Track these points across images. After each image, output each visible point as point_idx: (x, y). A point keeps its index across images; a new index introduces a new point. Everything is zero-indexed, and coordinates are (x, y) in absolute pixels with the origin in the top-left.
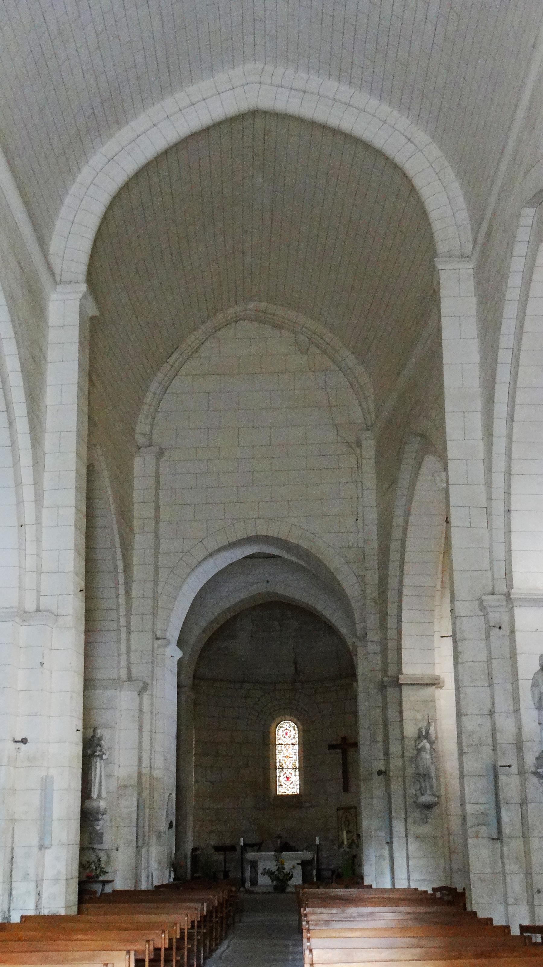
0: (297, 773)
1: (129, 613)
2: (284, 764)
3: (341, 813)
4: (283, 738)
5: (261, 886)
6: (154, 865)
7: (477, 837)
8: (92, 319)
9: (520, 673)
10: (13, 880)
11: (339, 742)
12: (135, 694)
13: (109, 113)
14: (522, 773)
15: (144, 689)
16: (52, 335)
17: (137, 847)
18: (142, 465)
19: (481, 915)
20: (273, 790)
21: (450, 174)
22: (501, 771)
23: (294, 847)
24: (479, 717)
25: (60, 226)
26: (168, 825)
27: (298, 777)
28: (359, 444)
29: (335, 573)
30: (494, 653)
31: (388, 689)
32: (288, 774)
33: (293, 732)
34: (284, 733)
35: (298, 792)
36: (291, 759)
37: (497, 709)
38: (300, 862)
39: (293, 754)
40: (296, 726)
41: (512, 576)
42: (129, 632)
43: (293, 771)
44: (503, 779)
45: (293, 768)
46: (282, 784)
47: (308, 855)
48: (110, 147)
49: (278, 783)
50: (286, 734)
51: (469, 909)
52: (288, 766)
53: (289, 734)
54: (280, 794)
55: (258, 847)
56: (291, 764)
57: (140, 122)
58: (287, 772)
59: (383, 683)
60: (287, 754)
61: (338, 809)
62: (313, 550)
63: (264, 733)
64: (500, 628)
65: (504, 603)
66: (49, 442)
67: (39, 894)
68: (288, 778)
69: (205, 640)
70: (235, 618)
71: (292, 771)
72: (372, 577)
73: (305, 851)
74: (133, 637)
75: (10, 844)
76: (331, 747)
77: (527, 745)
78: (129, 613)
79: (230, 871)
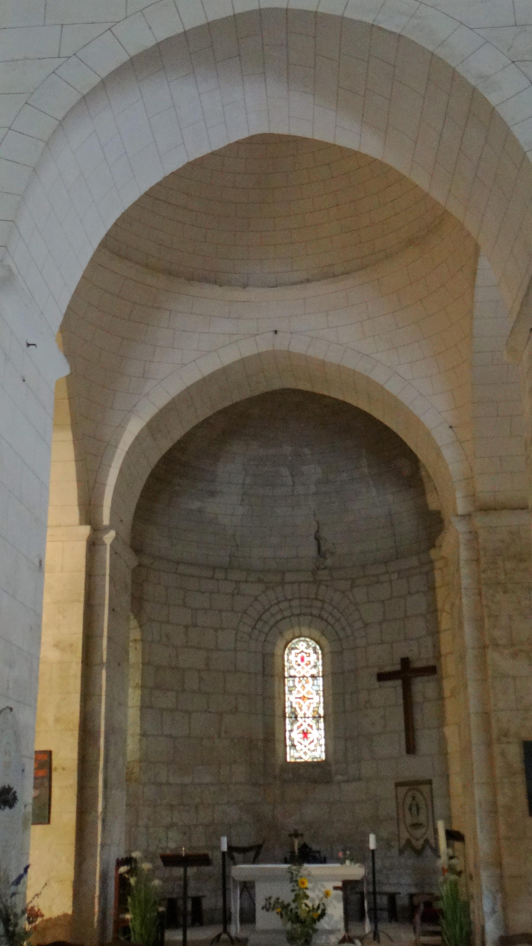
0: (322, 725)
2: (298, 710)
3: (403, 790)
4: (296, 666)
11: (398, 667)
20: (281, 755)
23: (319, 852)
27: (322, 732)
29: (481, 88)
32: (305, 727)
33: (313, 657)
35: (323, 757)
36: (311, 701)
38: (340, 884)
39: (315, 693)
40: (318, 647)
43: (314, 721)
45: (314, 717)
46: (296, 743)
47: (355, 871)
49: (288, 743)
50: (302, 659)
52: (305, 714)
53: (306, 659)
54: (293, 760)
55: (255, 853)
56: (311, 709)
58: (304, 723)
60: (303, 693)
61: (398, 785)
63: (264, 655)
68: (305, 734)
69: (155, 457)
71: (313, 722)
73: (348, 862)
76: (382, 677)
79: (203, 897)
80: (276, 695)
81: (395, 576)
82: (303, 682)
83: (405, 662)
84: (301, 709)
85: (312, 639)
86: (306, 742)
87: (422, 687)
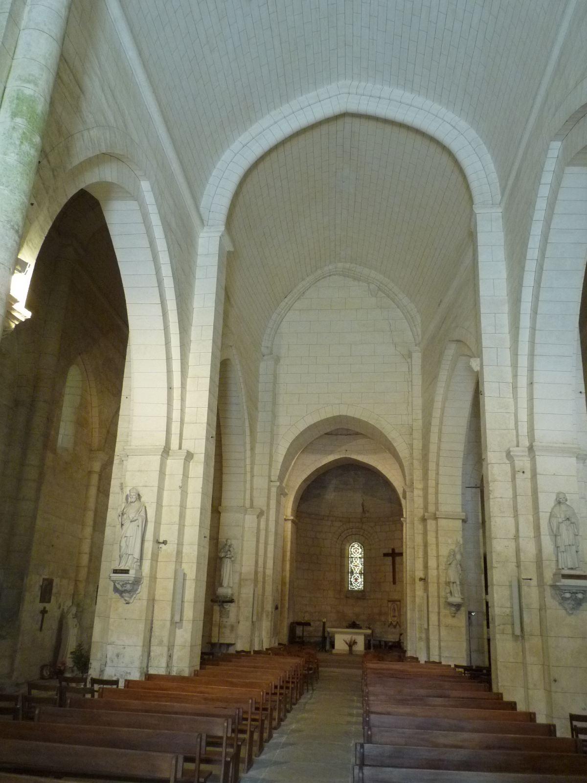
0: (363, 577)
1: (253, 463)
5: (337, 650)
6: (264, 634)
7: (503, 633)
8: (229, 252)
9: (540, 506)
10: (151, 644)
12: (255, 517)
13: (244, 112)
14: (541, 584)
15: (261, 514)
16: (200, 261)
17: (253, 622)
18: (265, 367)
19: (507, 698)
21: (484, 148)
22: (523, 583)
24: (506, 540)
25: (209, 189)
26: (274, 607)
27: (363, 579)
28: (410, 356)
29: (392, 441)
30: (519, 491)
31: (428, 521)
33: (360, 550)
34: (355, 551)
37: (521, 534)
41: (534, 433)
42: (252, 476)
44: (525, 589)
47: (369, 632)
48: (243, 138)
50: (356, 551)
51: (495, 690)
53: (358, 551)
57: (265, 122)
58: (356, 575)
59: (424, 517)
60: (356, 564)
62: (378, 426)
64: (523, 472)
65: (527, 454)
66: (194, 333)
67: (170, 656)
68: (356, 580)
70: (324, 474)
72: (418, 444)
74: (255, 479)
75: (150, 618)
76: (385, 555)
77: (545, 563)
78: (253, 463)
80: (346, 564)
81: (391, 523)
82: (356, 560)
83: (393, 550)
84: (355, 570)
85: (360, 543)
86: (357, 583)
87: (398, 559)
